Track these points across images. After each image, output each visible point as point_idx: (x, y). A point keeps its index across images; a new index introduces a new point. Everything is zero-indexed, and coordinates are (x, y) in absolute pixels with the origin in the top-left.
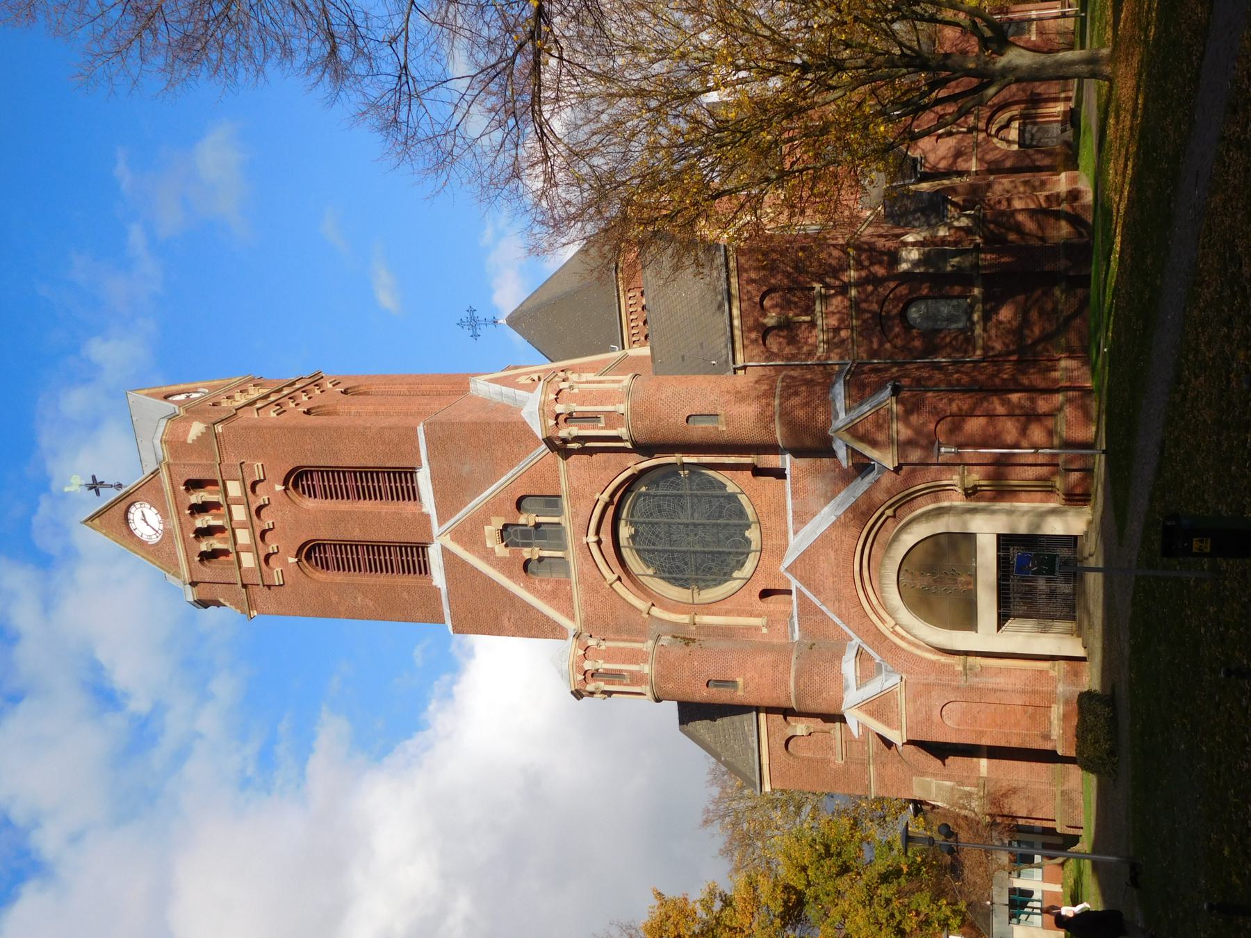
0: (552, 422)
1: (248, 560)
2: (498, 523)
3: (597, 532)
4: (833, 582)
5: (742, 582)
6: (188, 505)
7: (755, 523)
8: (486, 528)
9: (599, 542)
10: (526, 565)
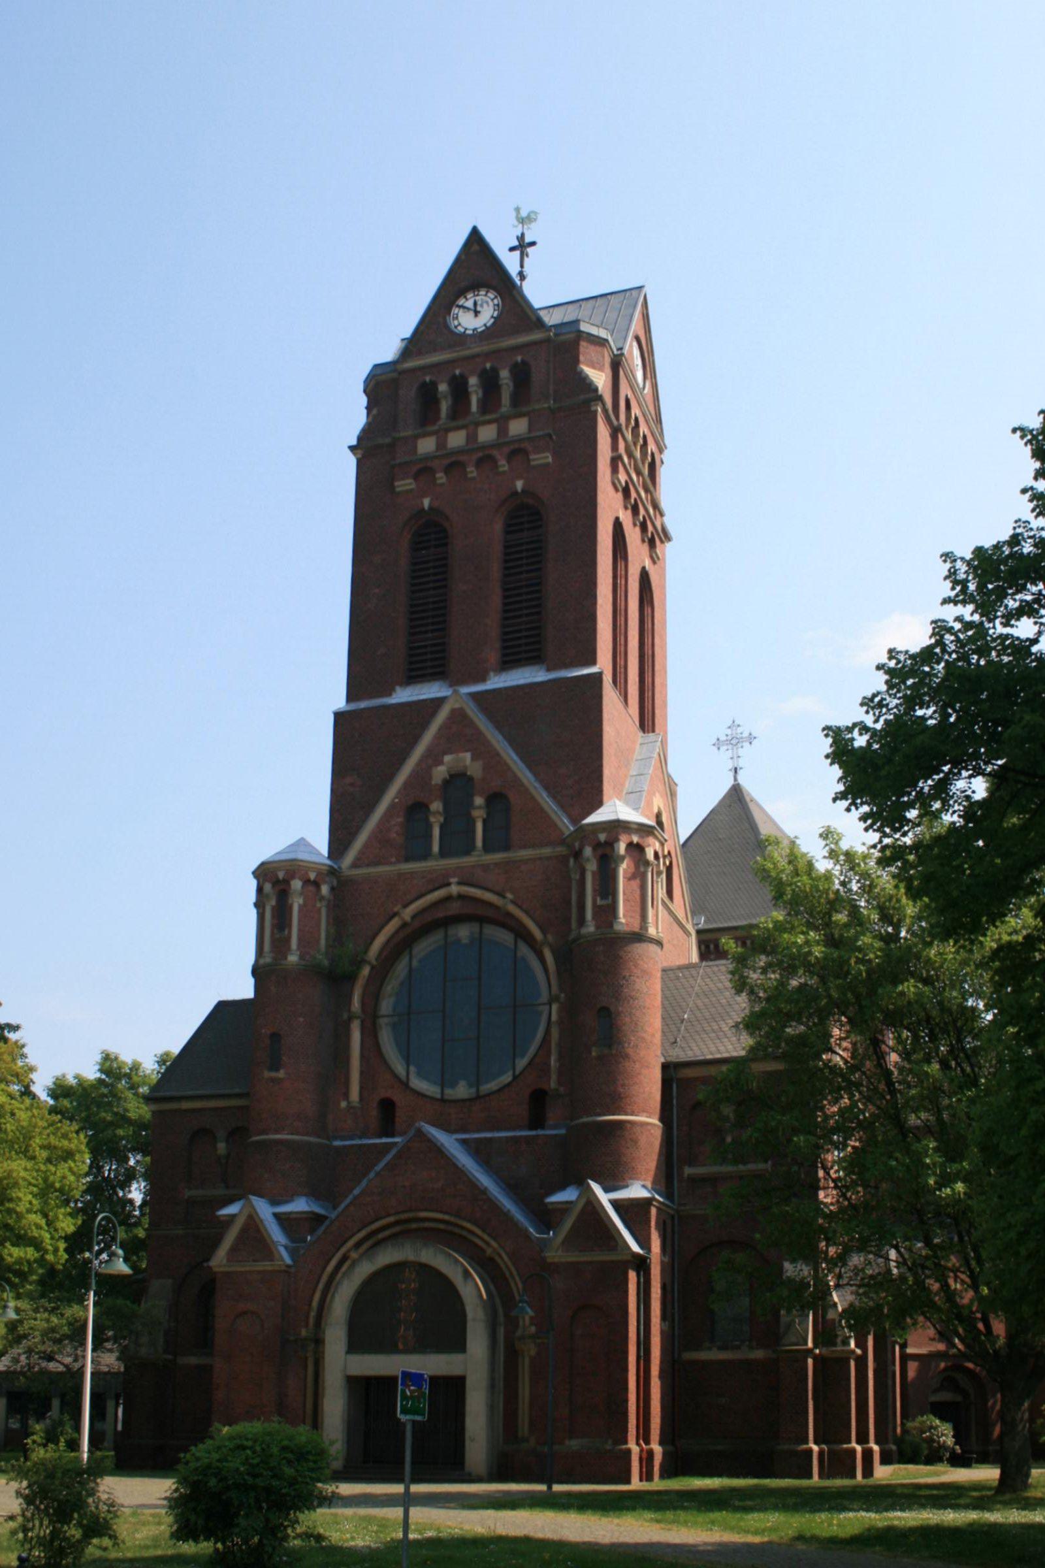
3: (461, 897)
8: (468, 755)
9: (449, 898)
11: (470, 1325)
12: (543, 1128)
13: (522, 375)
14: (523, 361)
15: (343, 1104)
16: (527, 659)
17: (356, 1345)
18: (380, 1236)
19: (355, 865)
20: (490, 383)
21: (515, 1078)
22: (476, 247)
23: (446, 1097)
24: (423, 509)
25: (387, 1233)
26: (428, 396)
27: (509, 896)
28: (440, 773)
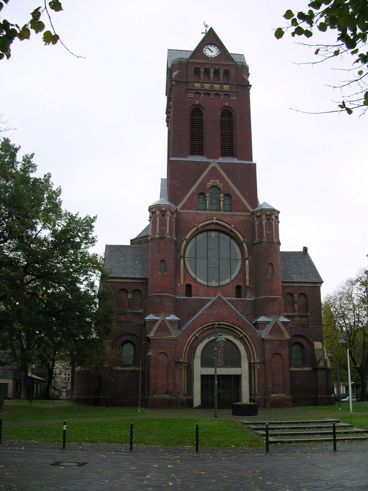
0: (259, 214)
1: (197, 85)
2: (221, 186)
3: (216, 224)
4: (214, 314)
5: (194, 278)
6: (219, 68)
7: (219, 284)
8: (218, 181)
9: (212, 223)
10: (203, 194)
11: (242, 359)
12: (191, 296)
13: (226, 73)
14: (218, 69)
15: (179, 285)
16: (229, 155)
17: (204, 364)
18: (205, 329)
19: (181, 209)
20: (216, 72)
21: (231, 281)
22: (211, 33)
23: (209, 285)
24: (226, 106)
25: (207, 328)
26: (197, 71)
27: (233, 226)
28: (209, 184)
